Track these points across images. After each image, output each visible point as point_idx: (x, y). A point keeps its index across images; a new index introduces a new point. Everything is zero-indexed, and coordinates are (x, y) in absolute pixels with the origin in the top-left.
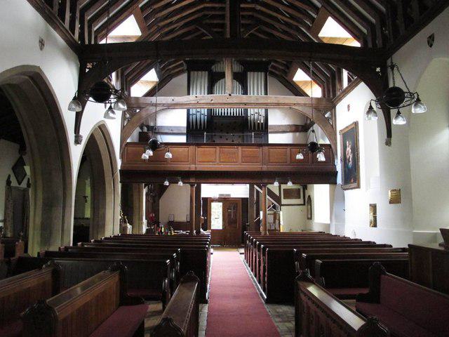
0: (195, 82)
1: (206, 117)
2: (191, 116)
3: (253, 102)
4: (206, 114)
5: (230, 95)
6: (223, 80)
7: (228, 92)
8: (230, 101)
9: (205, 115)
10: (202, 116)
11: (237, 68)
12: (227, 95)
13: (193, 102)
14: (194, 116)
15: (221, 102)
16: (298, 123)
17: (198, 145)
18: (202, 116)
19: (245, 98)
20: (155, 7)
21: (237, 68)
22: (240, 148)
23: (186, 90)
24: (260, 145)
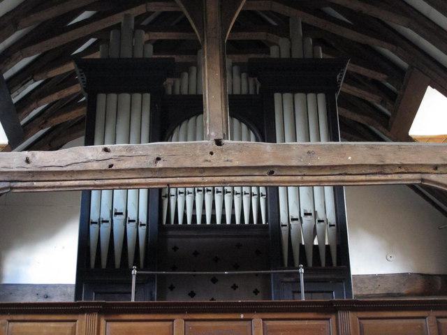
0: (111, 120)
1: (142, 230)
2: (93, 228)
3: (294, 163)
4: (143, 219)
5: (218, 142)
6: (200, 116)
7: (213, 133)
8: (218, 161)
9: (138, 224)
10: (131, 227)
11: (243, 85)
12: (210, 143)
13: (96, 166)
14: (105, 228)
15: (188, 164)
16: (431, 269)
17: (108, 311)
18: (131, 227)
19: (266, 153)
20: (54, 73)
21: (243, 85)
22: (257, 320)
23: (114, 231)
24: (330, 309)
